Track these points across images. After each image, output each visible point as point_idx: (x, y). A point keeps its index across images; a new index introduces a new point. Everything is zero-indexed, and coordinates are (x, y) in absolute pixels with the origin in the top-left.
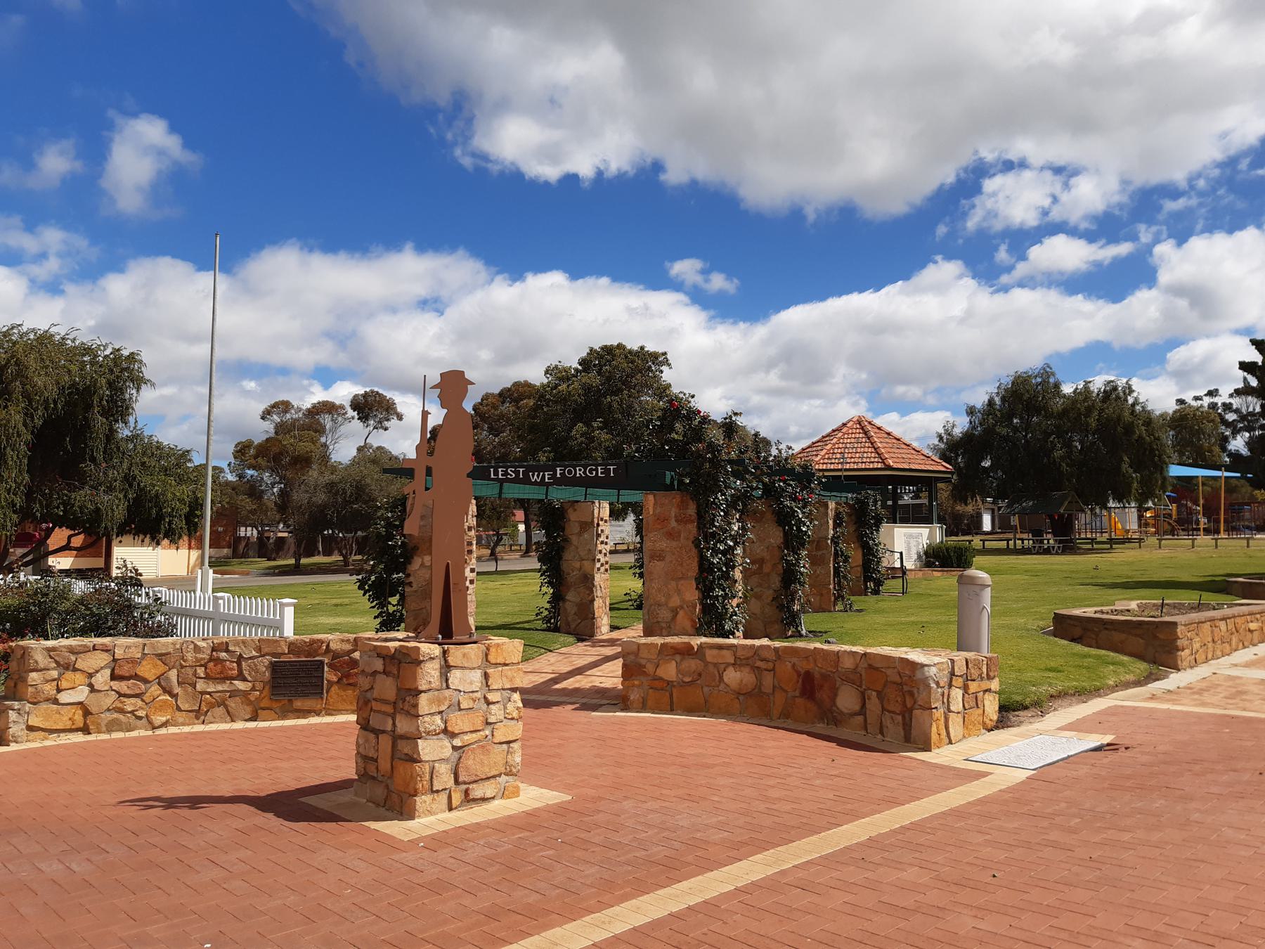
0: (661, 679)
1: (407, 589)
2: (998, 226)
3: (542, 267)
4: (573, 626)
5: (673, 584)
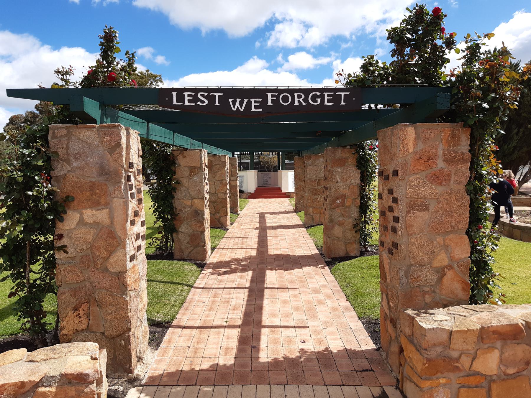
0: (477, 374)
1: (59, 255)
2: (280, 44)
3: (71, 45)
4: (186, 253)
5: (439, 239)
